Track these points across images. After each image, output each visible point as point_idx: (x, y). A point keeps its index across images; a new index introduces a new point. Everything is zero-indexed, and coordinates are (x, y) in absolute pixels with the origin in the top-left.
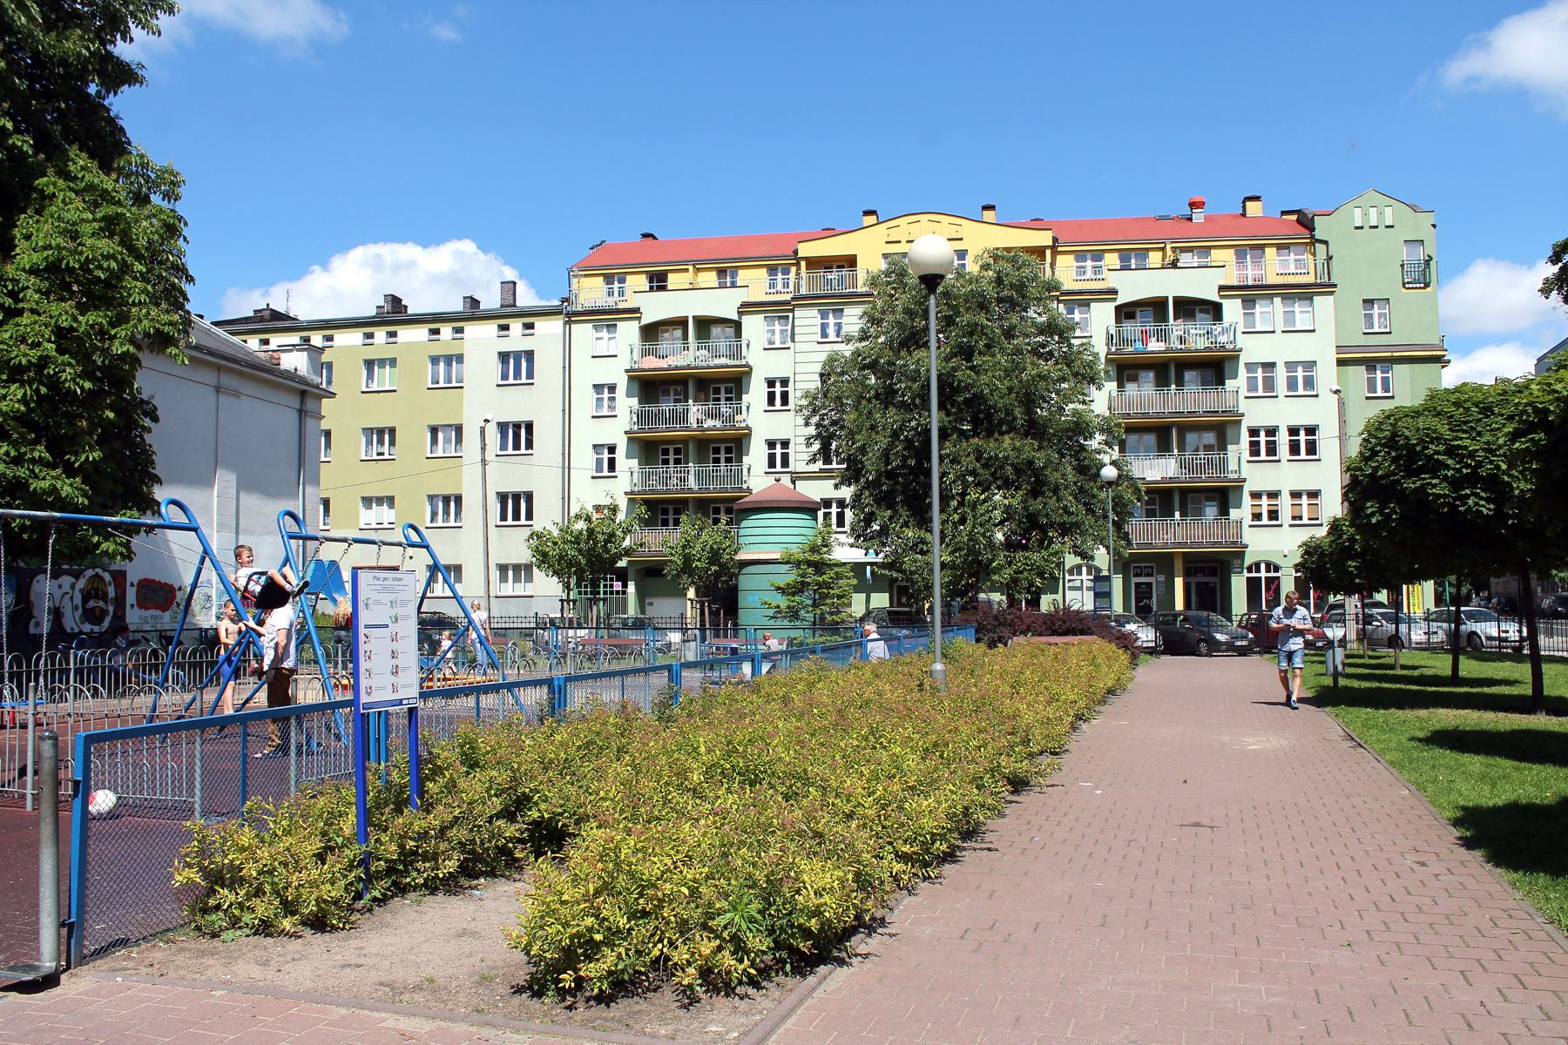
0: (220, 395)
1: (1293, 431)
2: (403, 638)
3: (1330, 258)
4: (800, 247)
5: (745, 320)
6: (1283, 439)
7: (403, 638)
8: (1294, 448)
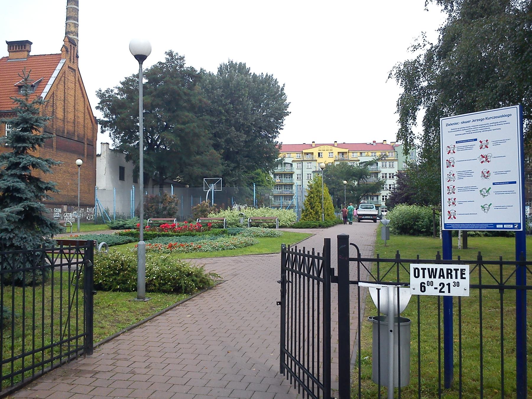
0: (154, 189)
1: (390, 174)
2: (460, 203)
3: (397, 154)
4: (303, 151)
5: (293, 163)
6: (388, 176)
7: (460, 203)
8: (390, 177)
